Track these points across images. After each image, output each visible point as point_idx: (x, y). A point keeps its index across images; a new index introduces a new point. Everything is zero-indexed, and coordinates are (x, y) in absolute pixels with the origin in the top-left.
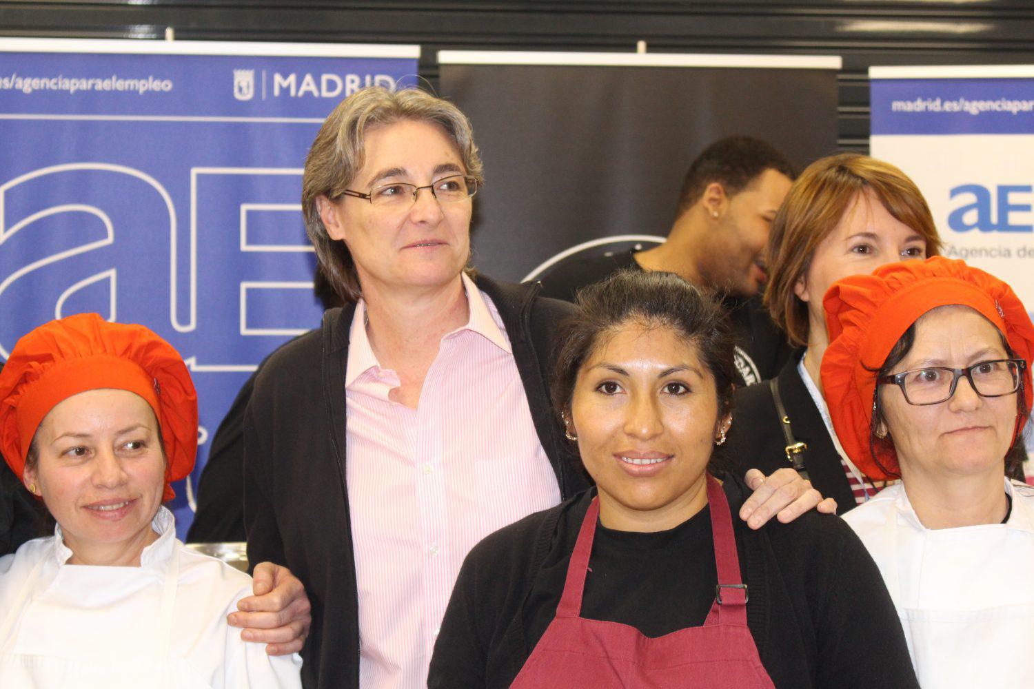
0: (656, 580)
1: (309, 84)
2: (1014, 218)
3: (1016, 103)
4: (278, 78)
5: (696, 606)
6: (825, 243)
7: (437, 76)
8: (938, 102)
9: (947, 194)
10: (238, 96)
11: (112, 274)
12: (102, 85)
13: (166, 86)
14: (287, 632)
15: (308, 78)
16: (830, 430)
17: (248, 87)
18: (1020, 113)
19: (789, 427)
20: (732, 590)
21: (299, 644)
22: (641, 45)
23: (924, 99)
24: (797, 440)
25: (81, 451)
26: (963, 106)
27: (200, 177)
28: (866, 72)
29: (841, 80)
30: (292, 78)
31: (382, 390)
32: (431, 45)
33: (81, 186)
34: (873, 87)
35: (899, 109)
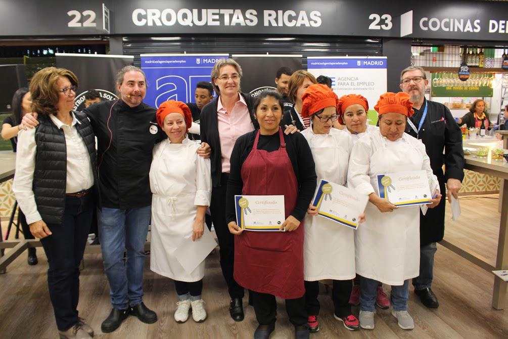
0: (270, 142)
4: (364, 62)
5: (277, 146)
11: (176, 95)
12: (337, 64)
14: (207, 154)
15: (209, 60)
20: (283, 144)
21: (209, 156)
22: (268, 53)
25: (171, 123)
31: (224, 112)
32: (231, 54)
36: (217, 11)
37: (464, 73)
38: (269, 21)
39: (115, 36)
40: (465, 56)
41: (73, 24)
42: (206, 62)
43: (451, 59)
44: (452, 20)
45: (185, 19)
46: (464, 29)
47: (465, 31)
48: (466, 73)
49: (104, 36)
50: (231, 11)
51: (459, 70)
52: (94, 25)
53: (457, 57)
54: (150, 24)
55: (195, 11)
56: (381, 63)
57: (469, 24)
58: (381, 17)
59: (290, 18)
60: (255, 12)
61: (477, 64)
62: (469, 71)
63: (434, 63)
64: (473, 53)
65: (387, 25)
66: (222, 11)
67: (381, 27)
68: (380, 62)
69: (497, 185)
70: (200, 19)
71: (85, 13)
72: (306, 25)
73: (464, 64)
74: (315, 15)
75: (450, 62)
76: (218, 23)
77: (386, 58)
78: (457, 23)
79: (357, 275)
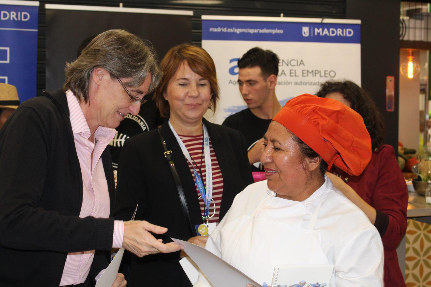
3: (253, 30)
4: (316, 30)
6: (171, 80)
7: (45, 14)
8: (226, 29)
9: (229, 61)
10: (304, 35)
12: (261, 31)
13: (281, 32)
15: (326, 30)
17: (307, 32)
18: (254, 33)
19: (165, 145)
22: (121, 4)
23: (221, 27)
24: (169, 150)
26: (235, 30)
27: (6, 51)
28: (200, 18)
29: (193, 21)
30: (321, 30)
34: (203, 23)
35: (212, 30)
42: (318, 34)
56: (349, 33)
68: (348, 30)
69: (422, 258)
77: (358, 22)
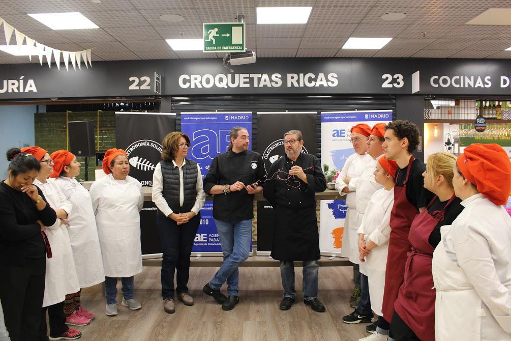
1: (376, 116)
2: (342, 135)
16: (150, 209)
33: (201, 133)
36: (247, 75)
37: (480, 125)
38: (12, 89)
39: (165, 96)
40: (481, 108)
41: (133, 87)
43: (469, 112)
44: (462, 77)
45: (221, 83)
46: (474, 85)
47: (476, 86)
48: (483, 125)
49: (156, 96)
50: (260, 75)
51: (475, 121)
52: (149, 88)
53: (473, 110)
54: (193, 86)
55: (230, 76)
56: (387, 116)
57: (479, 80)
58: (393, 77)
59: (310, 80)
60: (279, 76)
61: (494, 116)
62: (485, 123)
63: (450, 115)
64: (490, 106)
65: (399, 83)
66: (252, 75)
67: (393, 86)
70: (233, 82)
71: (142, 79)
72: (268, 86)
73: (480, 116)
74: (332, 77)
75: (466, 115)
76: (248, 86)
78: (467, 80)
79: (106, 277)
